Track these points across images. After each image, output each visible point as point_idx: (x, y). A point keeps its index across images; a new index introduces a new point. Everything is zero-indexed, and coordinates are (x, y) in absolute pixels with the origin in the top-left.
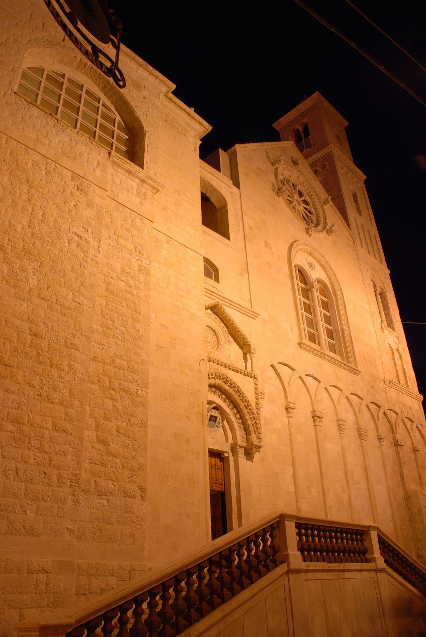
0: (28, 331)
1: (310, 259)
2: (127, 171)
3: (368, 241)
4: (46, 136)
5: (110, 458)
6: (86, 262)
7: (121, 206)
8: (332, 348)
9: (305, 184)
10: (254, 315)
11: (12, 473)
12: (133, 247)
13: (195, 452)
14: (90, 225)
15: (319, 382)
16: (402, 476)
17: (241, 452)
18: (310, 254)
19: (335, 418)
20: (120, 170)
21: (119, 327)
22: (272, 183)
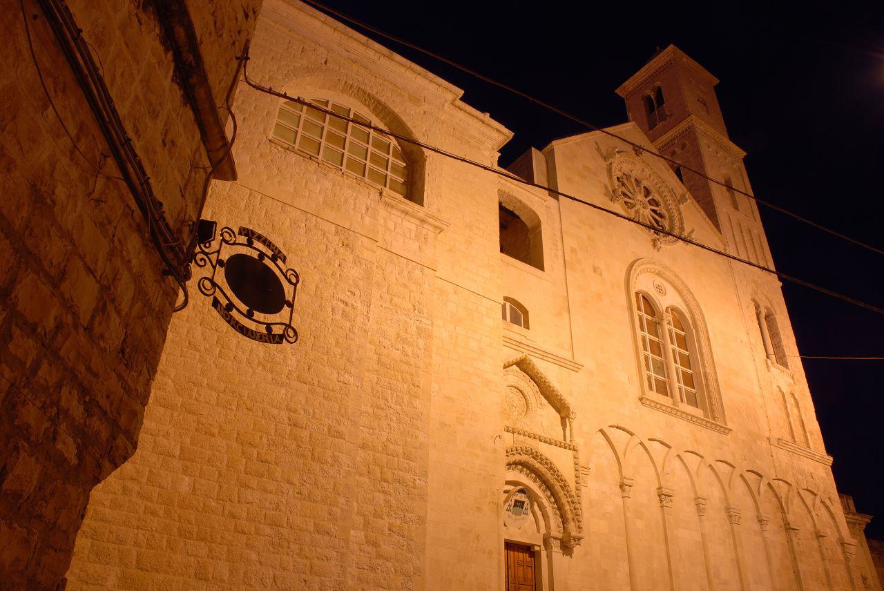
0: (286, 421)
1: (659, 281)
2: (403, 211)
3: (748, 245)
4: (306, 186)
5: (380, 562)
6: (353, 333)
7: (395, 257)
8: (693, 400)
9: (652, 178)
10: (576, 367)
11: (269, 582)
12: (410, 306)
13: (487, 551)
14: (357, 286)
15: (669, 447)
16: (797, 573)
17: (556, 545)
18: (658, 274)
19: (693, 496)
20: (394, 211)
21: (393, 405)
22: (604, 184)
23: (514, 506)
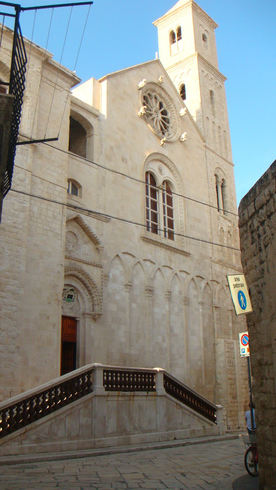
23: (67, 298)
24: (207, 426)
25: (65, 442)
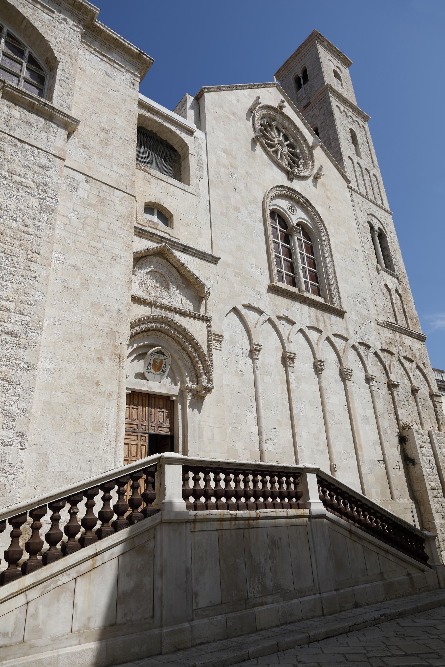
24: (416, 574)
25: (69, 650)
